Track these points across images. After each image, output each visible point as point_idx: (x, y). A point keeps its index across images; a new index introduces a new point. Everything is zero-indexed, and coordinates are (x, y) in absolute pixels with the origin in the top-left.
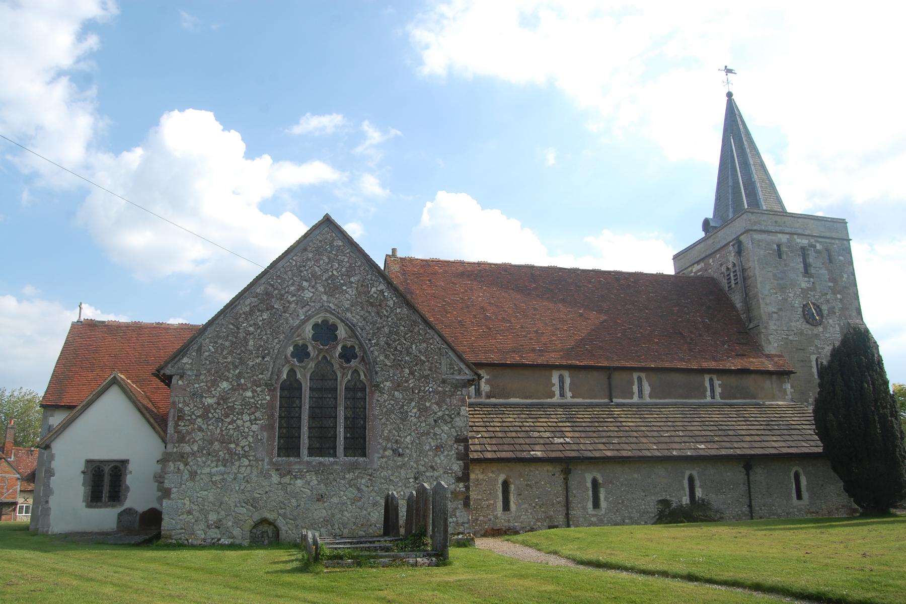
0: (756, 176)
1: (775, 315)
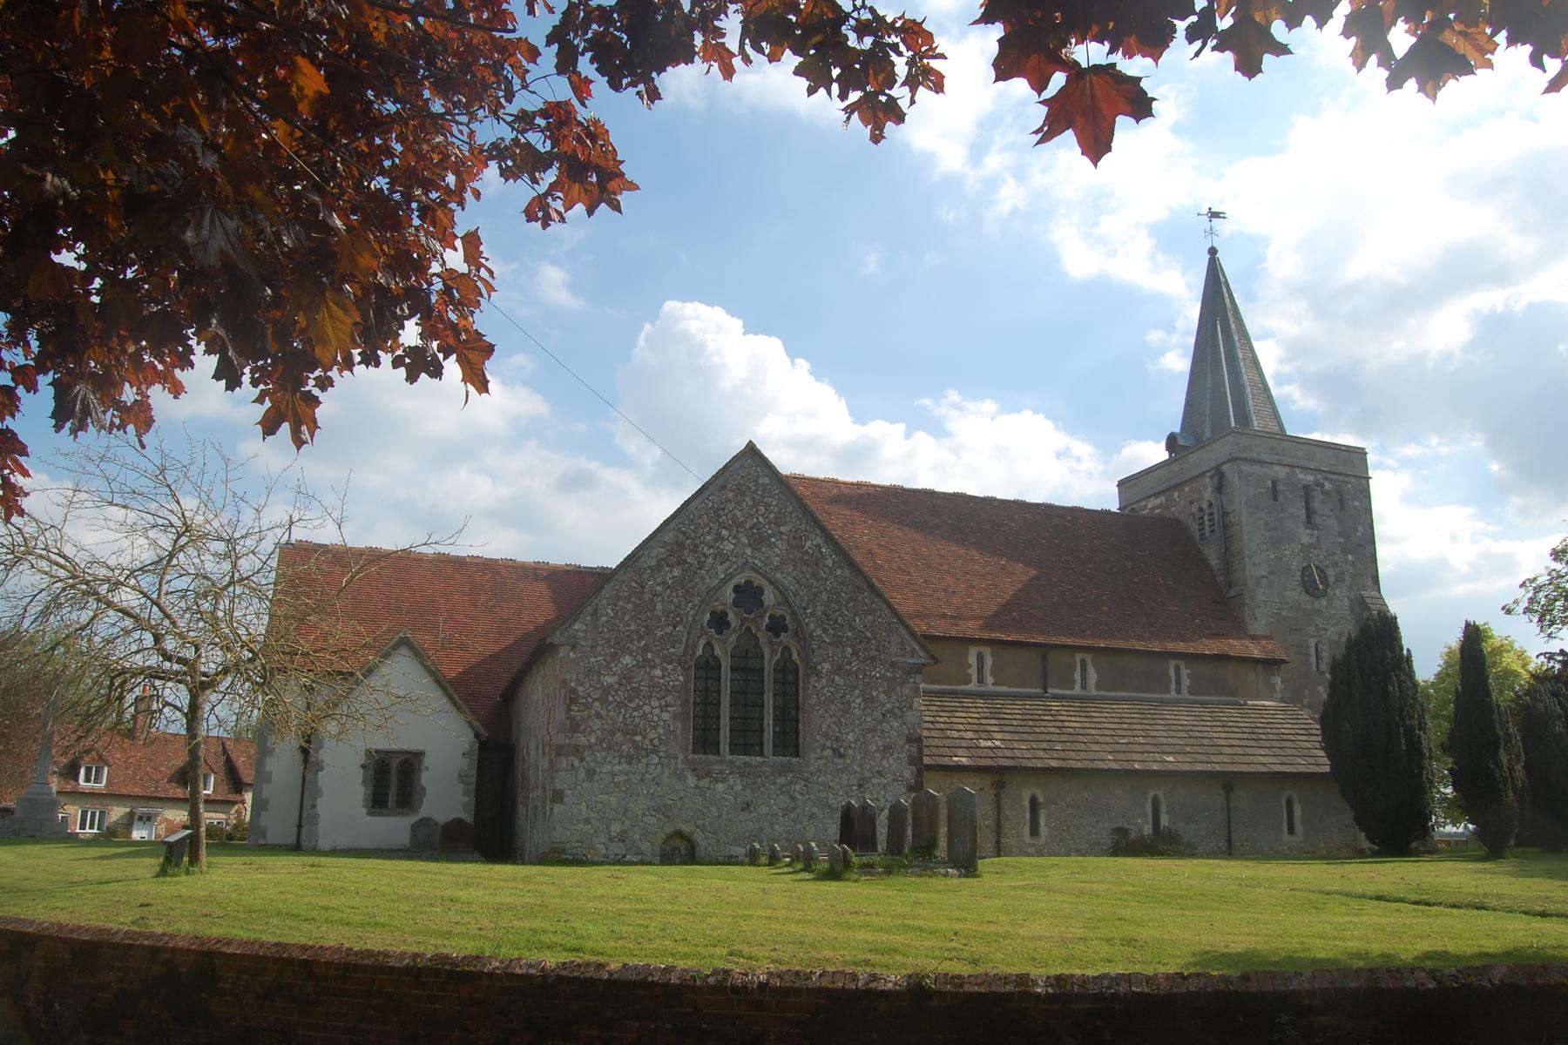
0: (1245, 377)
1: (1265, 581)
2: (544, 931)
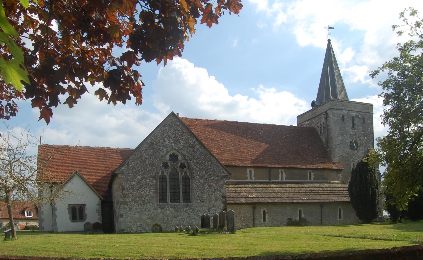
1: (338, 146)
2: (97, 251)
